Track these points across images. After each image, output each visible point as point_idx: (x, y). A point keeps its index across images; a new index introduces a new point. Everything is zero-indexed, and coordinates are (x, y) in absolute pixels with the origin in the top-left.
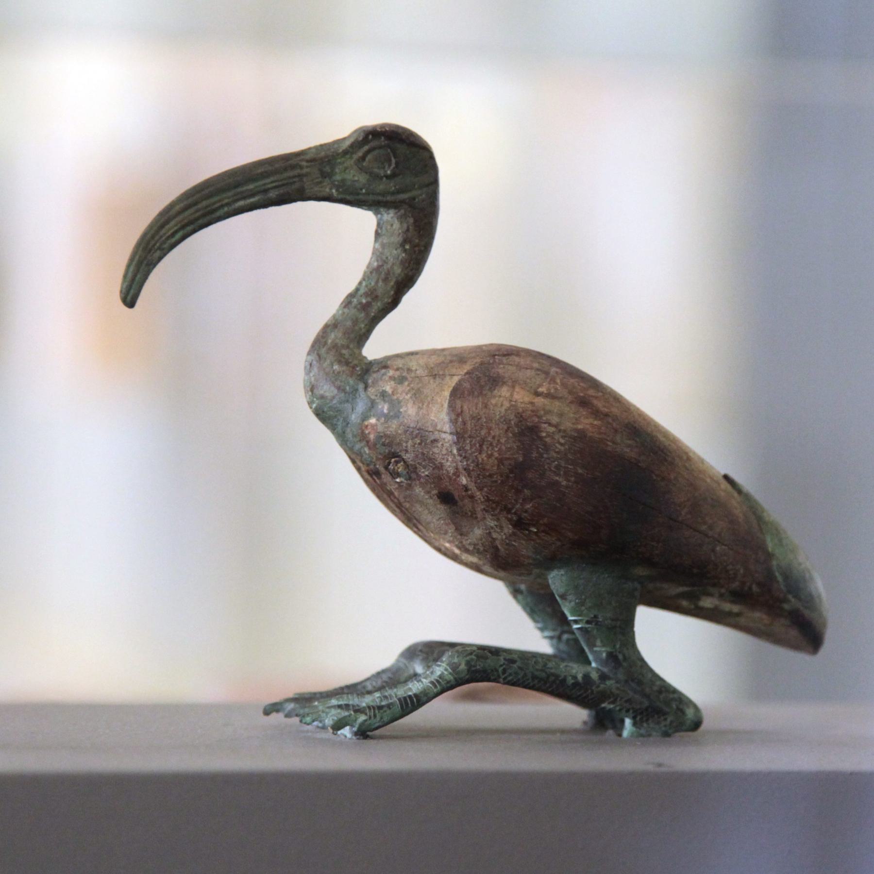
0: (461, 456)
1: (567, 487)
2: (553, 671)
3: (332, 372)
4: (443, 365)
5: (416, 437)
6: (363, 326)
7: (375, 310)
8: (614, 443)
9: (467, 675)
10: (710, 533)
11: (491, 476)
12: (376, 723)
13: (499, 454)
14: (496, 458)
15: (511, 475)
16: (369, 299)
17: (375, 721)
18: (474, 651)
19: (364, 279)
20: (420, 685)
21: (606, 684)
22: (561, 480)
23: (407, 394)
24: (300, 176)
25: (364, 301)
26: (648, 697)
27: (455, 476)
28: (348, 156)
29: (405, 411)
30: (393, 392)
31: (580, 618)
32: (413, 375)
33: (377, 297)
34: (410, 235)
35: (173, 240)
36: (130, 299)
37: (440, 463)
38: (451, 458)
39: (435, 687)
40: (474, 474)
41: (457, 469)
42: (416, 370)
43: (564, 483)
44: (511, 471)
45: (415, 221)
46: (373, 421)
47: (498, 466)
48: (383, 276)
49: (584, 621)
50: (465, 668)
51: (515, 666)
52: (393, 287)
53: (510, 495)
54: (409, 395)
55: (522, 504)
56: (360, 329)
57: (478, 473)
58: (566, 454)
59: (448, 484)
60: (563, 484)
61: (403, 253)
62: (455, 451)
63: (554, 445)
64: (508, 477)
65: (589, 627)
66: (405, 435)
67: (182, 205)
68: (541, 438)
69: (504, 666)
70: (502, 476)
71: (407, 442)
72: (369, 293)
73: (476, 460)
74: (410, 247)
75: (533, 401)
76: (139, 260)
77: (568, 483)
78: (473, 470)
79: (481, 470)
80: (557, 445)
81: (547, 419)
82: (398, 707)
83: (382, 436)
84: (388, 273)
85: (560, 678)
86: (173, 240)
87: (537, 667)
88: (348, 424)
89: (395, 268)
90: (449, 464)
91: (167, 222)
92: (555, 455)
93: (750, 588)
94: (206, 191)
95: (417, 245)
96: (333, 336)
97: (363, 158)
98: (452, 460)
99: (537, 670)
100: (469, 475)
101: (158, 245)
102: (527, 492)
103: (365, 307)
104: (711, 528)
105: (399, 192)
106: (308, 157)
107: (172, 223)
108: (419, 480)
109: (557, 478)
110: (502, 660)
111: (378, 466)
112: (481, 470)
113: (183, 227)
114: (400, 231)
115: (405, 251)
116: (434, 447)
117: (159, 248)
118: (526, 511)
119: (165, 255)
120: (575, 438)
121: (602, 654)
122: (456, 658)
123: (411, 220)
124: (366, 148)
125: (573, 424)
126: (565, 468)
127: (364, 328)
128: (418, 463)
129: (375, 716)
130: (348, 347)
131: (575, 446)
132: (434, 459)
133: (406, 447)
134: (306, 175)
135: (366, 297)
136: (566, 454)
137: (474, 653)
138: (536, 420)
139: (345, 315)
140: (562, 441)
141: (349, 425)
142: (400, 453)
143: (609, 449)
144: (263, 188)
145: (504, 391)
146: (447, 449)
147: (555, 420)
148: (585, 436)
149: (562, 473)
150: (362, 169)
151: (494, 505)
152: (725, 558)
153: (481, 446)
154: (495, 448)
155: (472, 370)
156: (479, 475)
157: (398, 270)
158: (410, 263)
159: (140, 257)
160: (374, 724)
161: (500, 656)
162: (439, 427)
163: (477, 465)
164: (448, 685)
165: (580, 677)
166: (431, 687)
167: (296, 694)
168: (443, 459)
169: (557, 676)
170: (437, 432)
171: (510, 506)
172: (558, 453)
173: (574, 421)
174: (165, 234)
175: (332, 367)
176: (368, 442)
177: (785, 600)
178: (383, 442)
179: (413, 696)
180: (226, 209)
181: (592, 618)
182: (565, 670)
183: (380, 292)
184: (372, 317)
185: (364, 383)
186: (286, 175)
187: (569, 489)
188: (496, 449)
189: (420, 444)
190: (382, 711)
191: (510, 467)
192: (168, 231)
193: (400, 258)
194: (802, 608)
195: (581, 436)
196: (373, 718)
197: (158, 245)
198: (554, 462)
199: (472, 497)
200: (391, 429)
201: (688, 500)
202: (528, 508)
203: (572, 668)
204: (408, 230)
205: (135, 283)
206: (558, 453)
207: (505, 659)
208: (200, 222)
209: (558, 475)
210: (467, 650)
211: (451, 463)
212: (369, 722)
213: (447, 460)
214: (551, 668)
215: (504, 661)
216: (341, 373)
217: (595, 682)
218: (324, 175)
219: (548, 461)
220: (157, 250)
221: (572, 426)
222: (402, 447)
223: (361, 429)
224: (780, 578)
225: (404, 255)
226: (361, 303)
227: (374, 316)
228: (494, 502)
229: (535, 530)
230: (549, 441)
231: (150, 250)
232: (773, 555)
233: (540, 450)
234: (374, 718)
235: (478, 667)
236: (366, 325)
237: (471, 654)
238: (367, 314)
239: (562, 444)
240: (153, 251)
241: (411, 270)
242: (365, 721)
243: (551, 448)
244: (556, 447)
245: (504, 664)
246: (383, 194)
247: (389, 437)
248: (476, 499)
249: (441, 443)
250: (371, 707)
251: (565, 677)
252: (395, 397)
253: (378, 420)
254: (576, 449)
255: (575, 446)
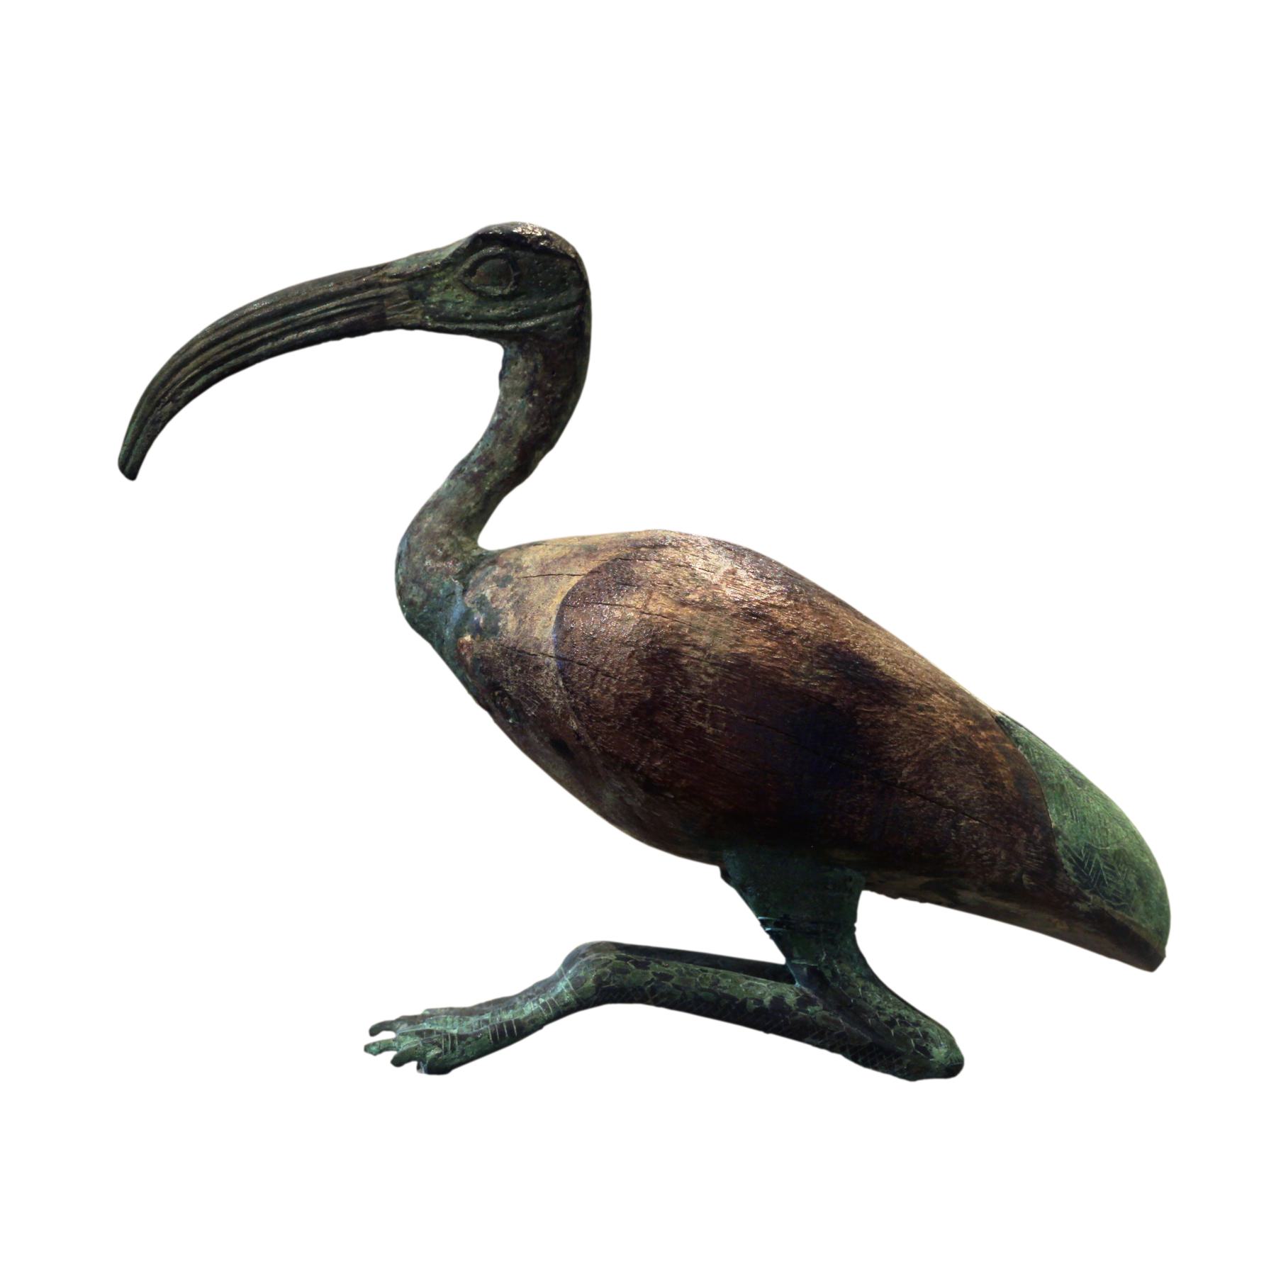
0: (567, 690)
1: (714, 736)
2: (726, 992)
3: (423, 568)
4: (563, 560)
5: (516, 661)
6: (472, 504)
7: (491, 483)
8: (793, 673)
9: (595, 994)
10: (951, 802)
11: (607, 719)
12: (455, 1058)
13: (618, 689)
14: (614, 695)
15: (634, 719)
16: (482, 467)
17: (453, 1056)
18: (611, 961)
19: (482, 440)
20: (535, 1006)
21: (807, 1012)
22: (705, 725)
23: (508, 601)
24: (380, 298)
25: (476, 470)
26: (871, 1030)
27: (564, 718)
28: (449, 269)
29: (504, 625)
30: (492, 598)
31: (767, 918)
32: (521, 574)
33: (493, 463)
34: (538, 378)
35: (192, 388)
36: (130, 464)
37: (546, 699)
38: (557, 692)
39: (548, 1010)
40: (585, 716)
41: (565, 708)
42: (528, 567)
43: (710, 730)
44: (635, 713)
45: (545, 358)
46: (468, 638)
47: (616, 705)
48: (503, 435)
49: (773, 922)
50: (594, 985)
51: (669, 984)
52: (515, 450)
53: (634, 747)
54: (511, 604)
55: (650, 760)
56: (469, 508)
57: (590, 714)
58: (715, 690)
59: (557, 729)
60: (708, 731)
61: (530, 403)
62: (561, 683)
63: (698, 676)
64: (629, 720)
65: (779, 931)
66: (504, 659)
67: (206, 341)
68: (679, 667)
69: (653, 983)
70: (621, 720)
71: (506, 669)
72: (484, 459)
73: (586, 697)
74: (539, 394)
75: (676, 613)
76: (142, 417)
77: (716, 730)
78: (583, 711)
79: (594, 711)
80: (703, 676)
81: (693, 640)
82: (489, 1038)
83: (478, 659)
84: (509, 432)
85: (737, 1002)
86: (192, 388)
87: (704, 987)
88: (443, 641)
89: (520, 424)
90: (555, 700)
91: (185, 363)
92: (698, 691)
93: (1020, 880)
94: (242, 322)
95: (551, 392)
96: (430, 519)
97: (471, 271)
98: (559, 696)
99: (702, 990)
100: (579, 718)
101: (170, 394)
102: (657, 744)
103: (475, 479)
104: (952, 794)
105: (521, 318)
106: (393, 271)
107: (192, 365)
108: (528, 722)
109: (700, 723)
110: (650, 974)
111: (487, 701)
112: (594, 711)
113: (206, 370)
114: (526, 372)
115: (532, 400)
116: (538, 677)
117: (171, 399)
118: (656, 770)
119: (179, 409)
120: (731, 667)
121: (802, 969)
122: (583, 971)
123: (539, 357)
124: (475, 257)
125: (731, 646)
126: (712, 708)
127: (474, 507)
128: (522, 698)
129: (453, 1049)
130: (449, 534)
131: (731, 679)
132: (538, 693)
133: (507, 675)
134: (390, 295)
135: (480, 464)
136: (715, 690)
137: (611, 965)
138: (676, 640)
139: (451, 489)
140: (711, 671)
141: (445, 643)
142: (501, 685)
143: (784, 682)
144: (322, 315)
145: (636, 599)
146: (552, 680)
147: (705, 639)
148: (748, 664)
149: (707, 715)
150: (467, 287)
151: (613, 760)
152: (976, 837)
153: (593, 676)
154: (613, 680)
155: (599, 568)
156: (590, 717)
157: (522, 428)
158: (539, 416)
159: (144, 412)
160: (453, 1059)
161: (649, 968)
162: (542, 650)
163: (588, 704)
164: (566, 1009)
165: (767, 1001)
166: (541, 1011)
167: (428, 1010)
168: (549, 694)
169: (733, 999)
170: (540, 657)
171: (633, 762)
172: (703, 687)
173: (733, 642)
174: (180, 380)
175: (424, 562)
176: (466, 666)
177: (1079, 897)
178: (481, 668)
179: (513, 1023)
180: (270, 345)
181: (781, 918)
182: (746, 990)
183: (497, 457)
184: (485, 492)
185: (464, 584)
186: (357, 296)
187: (717, 739)
188: (614, 682)
189: (521, 672)
190: (464, 1042)
191: (633, 707)
192: (186, 376)
193: (526, 409)
194: (1107, 908)
195: (743, 664)
196: (450, 1052)
197: (170, 394)
198: (696, 700)
199: (586, 748)
200: (488, 650)
201: (916, 754)
202: (659, 766)
203: (758, 987)
204: (536, 370)
205: (136, 447)
206: (703, 687)
207: (655, 974)
208: (233, 362)
209: (703, 719)
210: (601, 959)
211: (558, 700)
212: (444, 1057)
213: (554, 696)
214: (725, 988)
215: (653, 976)
216: (435, 570)
217: (790, 1007)
218: (415, 296)
219: (689, 699)
220: (168, 402)
221: (729, 649)
222: (502, 677)
223: (456, 649)
224: (1068, 866)
225: (531, 405)
226: (471, 473)
227: (490, 491)
228: (612, 755)
229: (672, 796)
230: (692, 671)
231: (158, 403)
232: (1059, 833)
233: (678, 683)
234: (453, 1052)
235: (612, 984)
236: (477, 503)
237: (605, 965)
238: (479, 489)
239: (709, 675)
240: (162, 404)
241: (543, 426)
242: (439, 1055)
243: (694, 681)
244: (702, 680)
245: (652, 980)
246: (500, 320)
247: (486, 661)
248: (591, 750)
249: (546, 671)
250: (449, 1037)
251: (745, 1001)
252: (494, 606)
253: (473, 637)
254: (731, 682)
255: (731, 679)
